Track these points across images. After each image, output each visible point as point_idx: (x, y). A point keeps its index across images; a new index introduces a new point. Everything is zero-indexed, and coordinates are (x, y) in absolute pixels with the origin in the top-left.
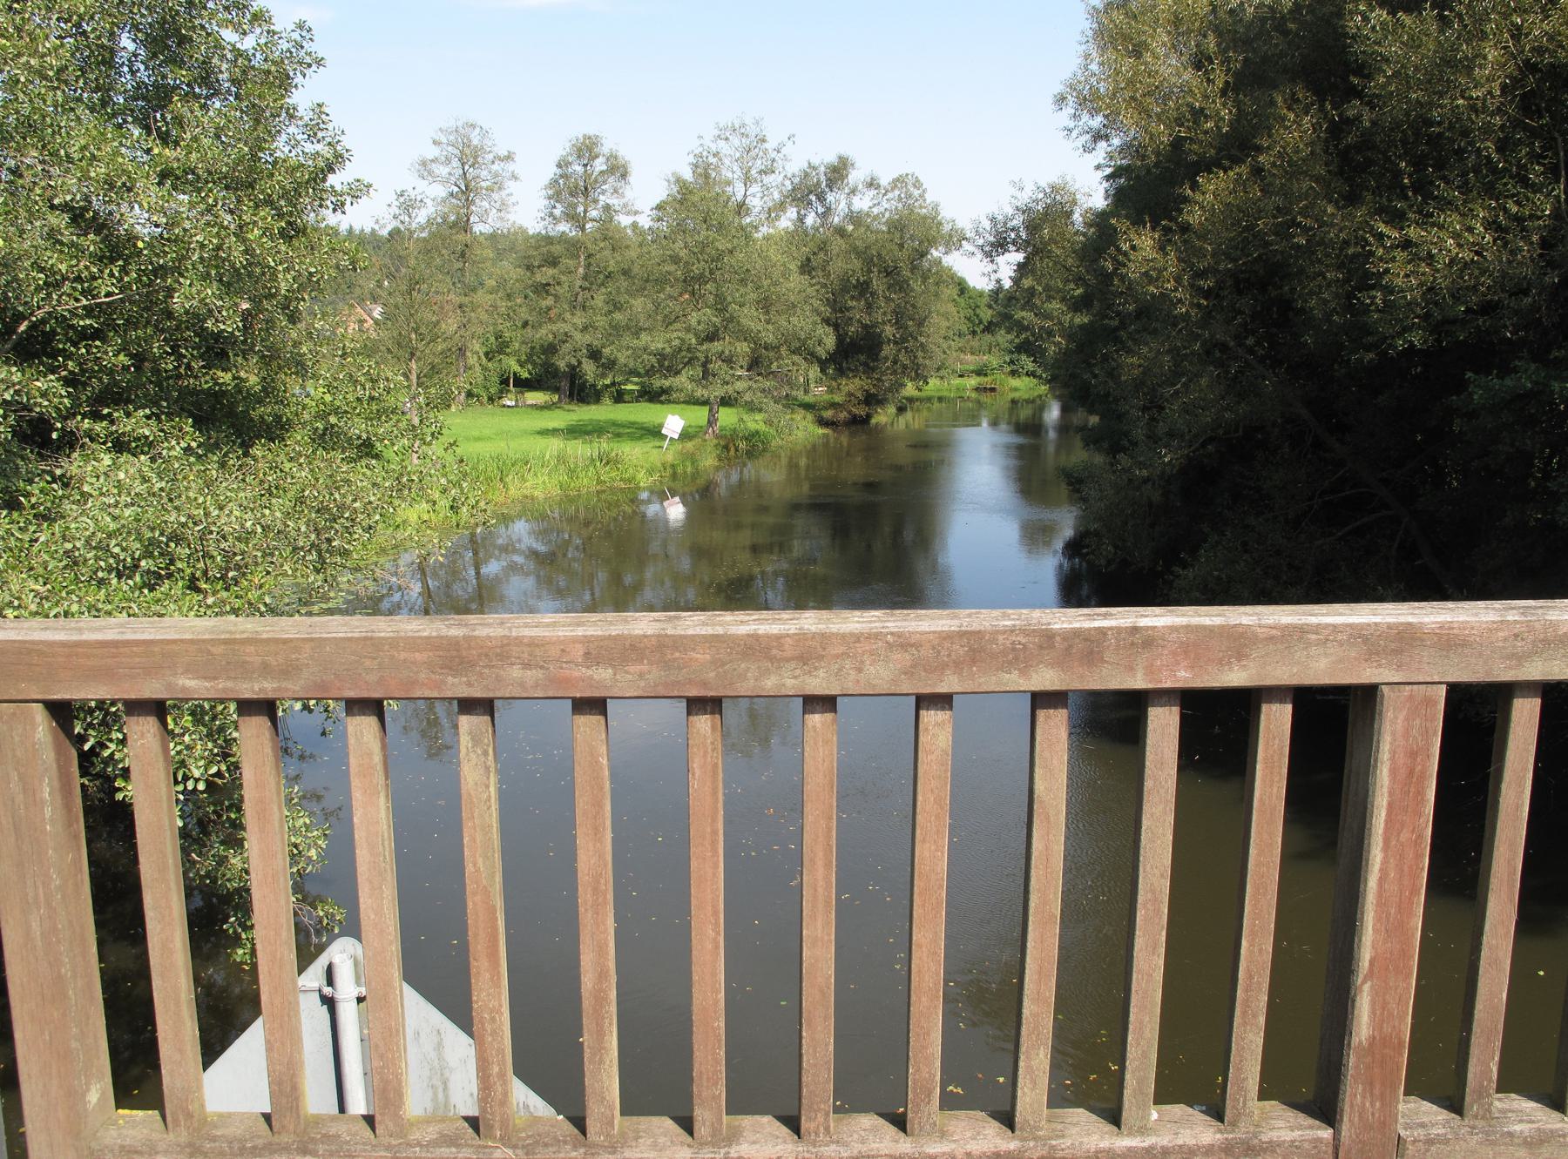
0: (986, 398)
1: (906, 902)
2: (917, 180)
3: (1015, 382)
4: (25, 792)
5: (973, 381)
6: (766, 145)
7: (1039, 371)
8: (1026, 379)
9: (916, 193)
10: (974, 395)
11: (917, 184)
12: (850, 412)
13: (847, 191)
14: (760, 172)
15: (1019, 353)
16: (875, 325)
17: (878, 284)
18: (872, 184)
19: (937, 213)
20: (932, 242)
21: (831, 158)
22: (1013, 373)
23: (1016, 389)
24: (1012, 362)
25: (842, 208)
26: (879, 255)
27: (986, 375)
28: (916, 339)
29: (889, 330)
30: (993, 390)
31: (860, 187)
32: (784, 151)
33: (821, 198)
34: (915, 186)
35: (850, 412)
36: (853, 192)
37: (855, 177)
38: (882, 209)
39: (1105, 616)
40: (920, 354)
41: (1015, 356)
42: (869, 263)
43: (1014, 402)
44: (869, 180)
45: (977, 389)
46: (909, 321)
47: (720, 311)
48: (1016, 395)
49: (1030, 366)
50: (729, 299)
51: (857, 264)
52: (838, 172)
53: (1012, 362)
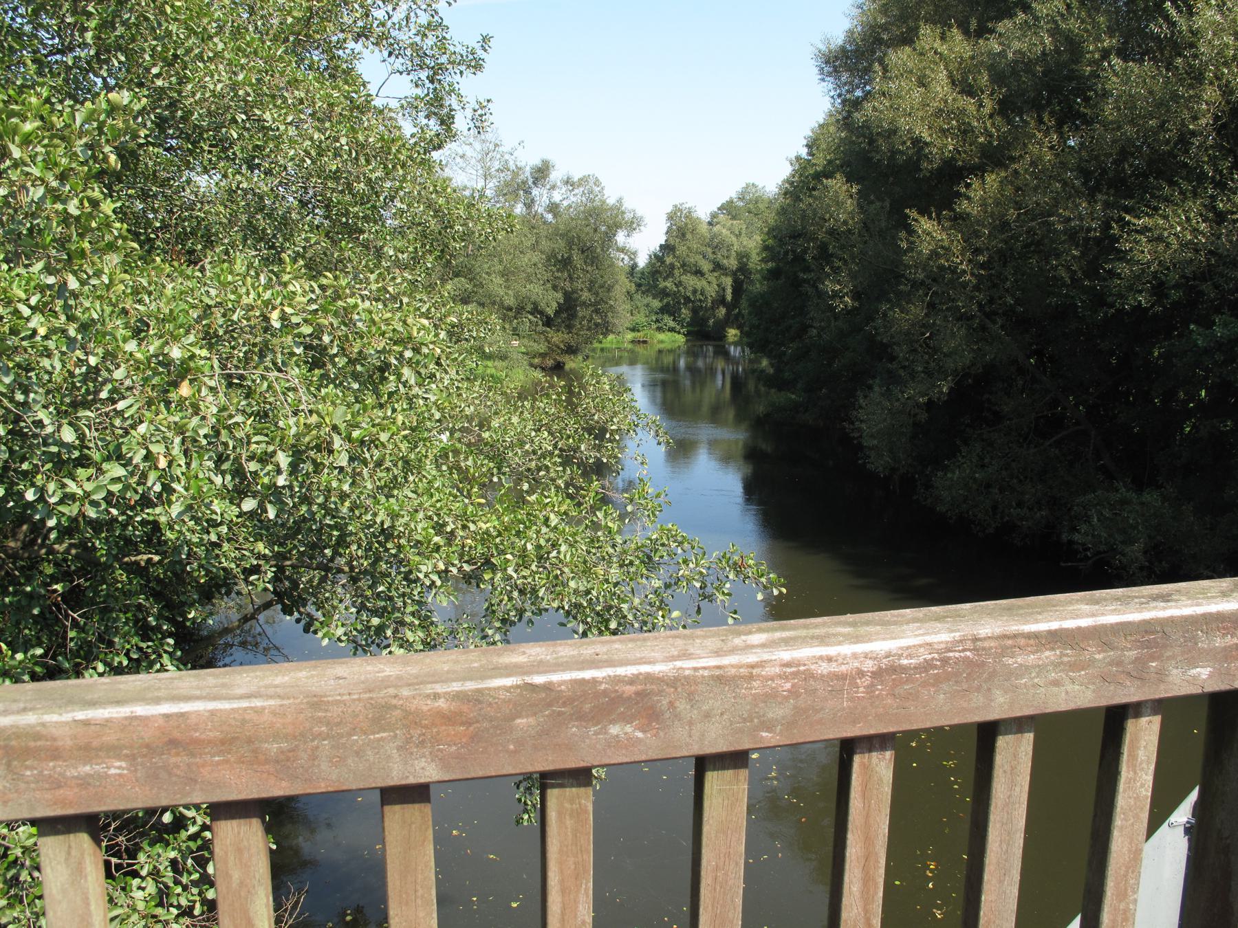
0: (640, 349)
1: (658, 764)
2: (597, 180)
3: (661, 336)
4: (223, 742)
5: (630, 336)
6: (501, 149)
7: (678, 328)
8: (670, 334)
9: (597, 189)
10: (630, 346)
11: (597, 183)
12: (555, 360)
13: (548, 187)
14: (497, 171)
15: (663, 314)
16: (574, 292)
17: (577, 258)
18: (567, 182)
19: (621, 205)
20: (618, 226)
21: (536, 161)
22: (659, 329)
23: (662, 342)
24: (657, 321)
25: (545, 201)
26: (579, 237)
27: (638, 331)
28: (607, 303)
29: (586, 296)
30: (645, 342)
31: (559, 184)
32: (515, 154)
33: (528, 192)
34: (595, 184)
35: (555, 360)
36: (553, 187)
37: (555, 176)
38: (570, 202)
39: (1165, 598)
40: (610, 314)
41: (660, 316)
42: (570, 244)
43: (660, 351)
44: (565, 178)
45: (633, 342)
46: (602, 290)
47: (471, 280)
48: (661, 346)
49: (672, 324)
50: (478, 270)
51: (561, 243)
52: (541, 173)
53: (657, 321)
